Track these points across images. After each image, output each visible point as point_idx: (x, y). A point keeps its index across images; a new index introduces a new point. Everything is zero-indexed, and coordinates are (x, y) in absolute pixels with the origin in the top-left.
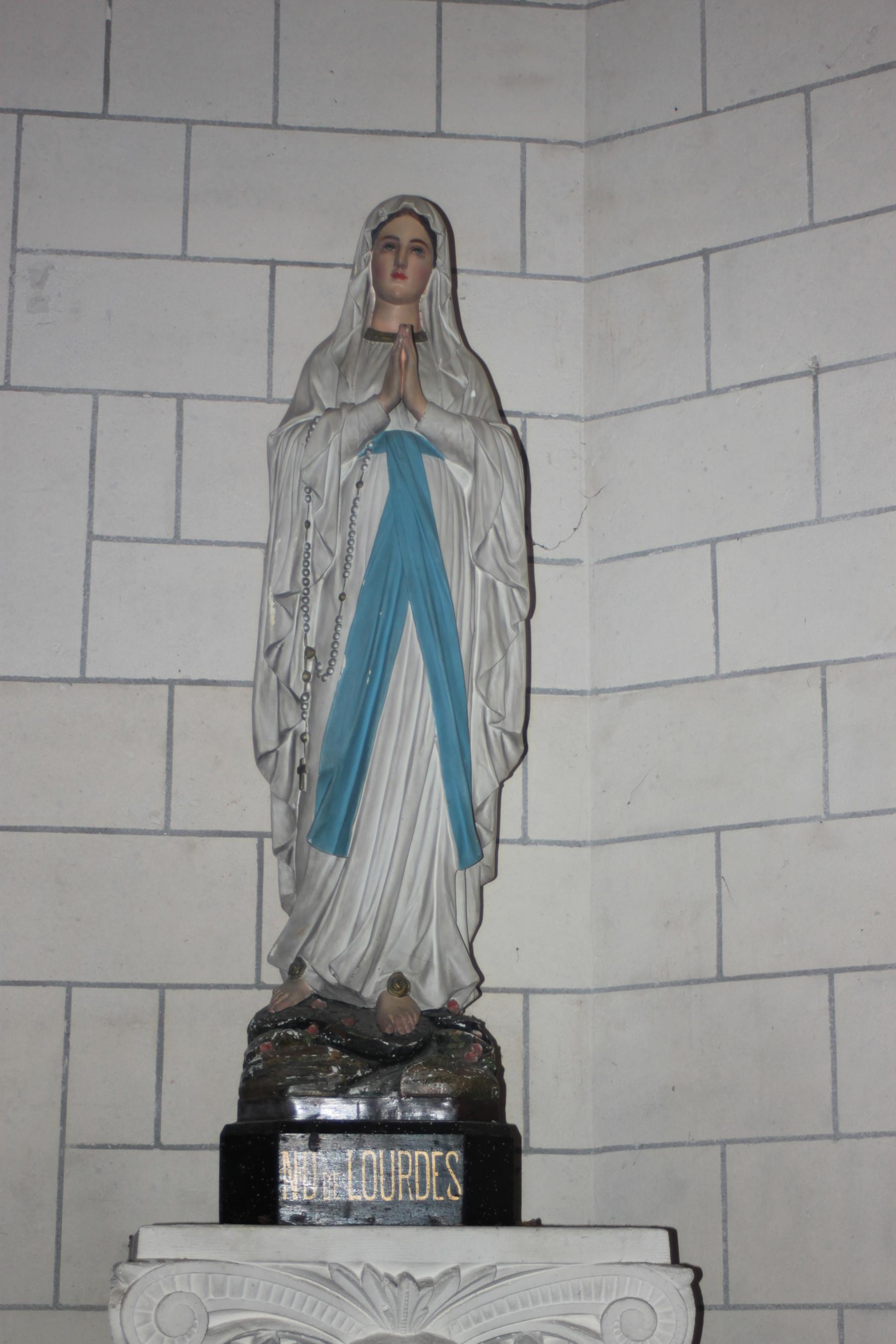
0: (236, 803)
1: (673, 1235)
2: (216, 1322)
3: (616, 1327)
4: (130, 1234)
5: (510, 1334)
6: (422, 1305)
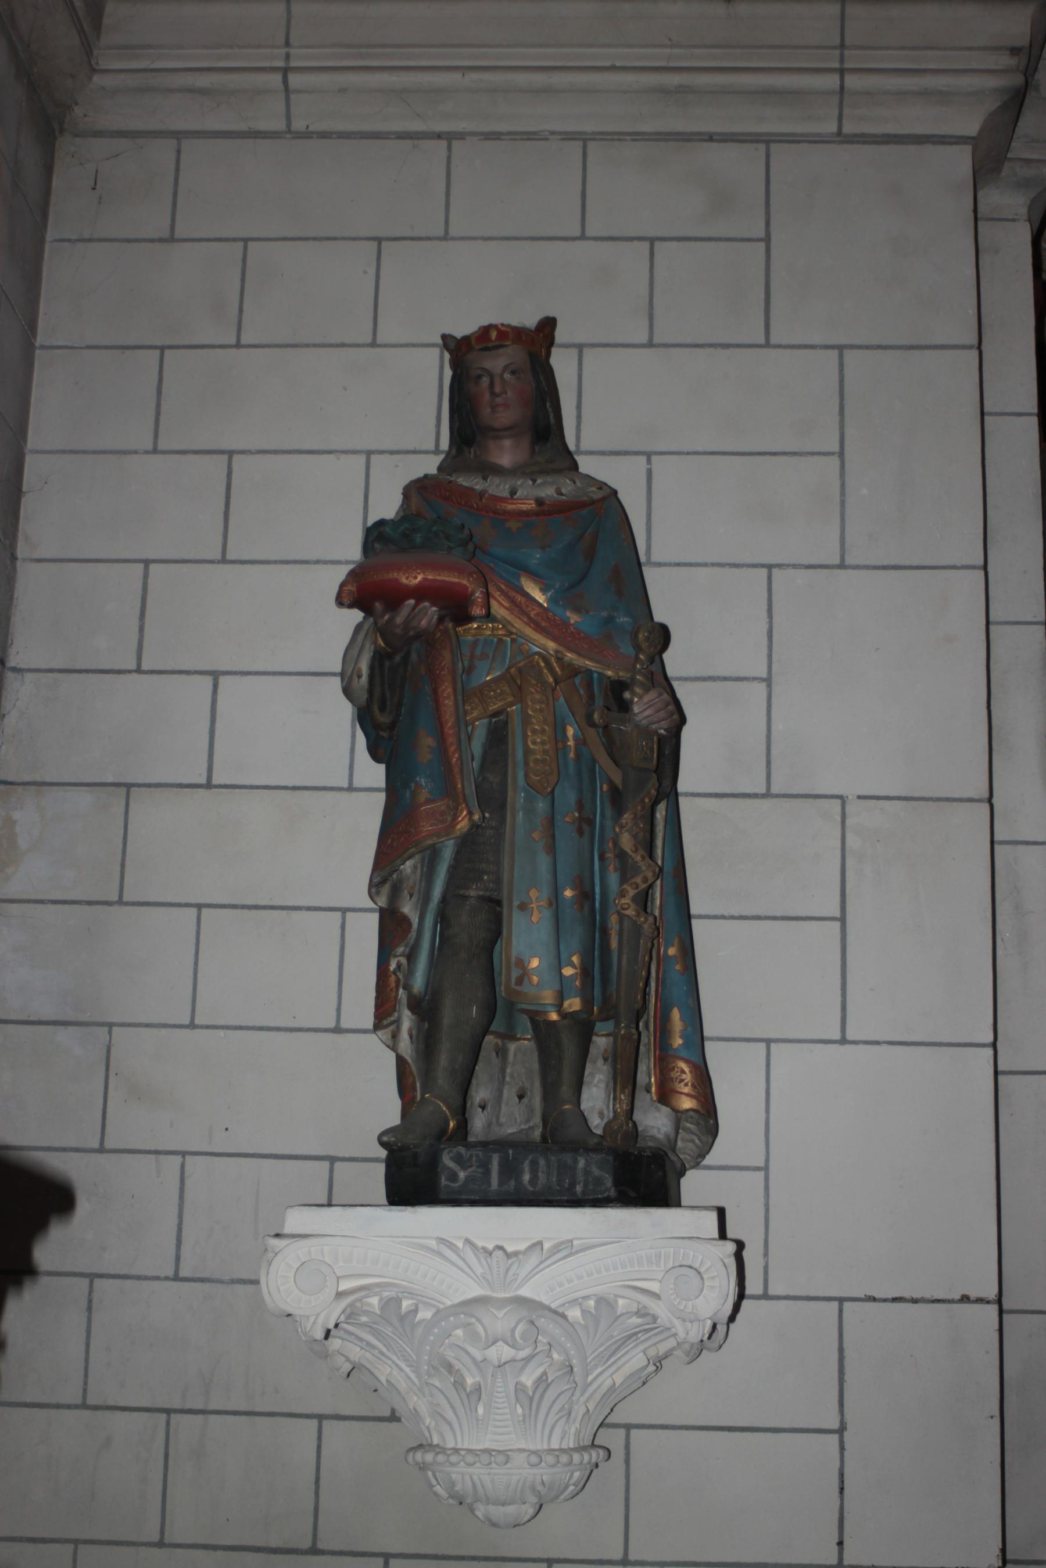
0: (490, 1520)
1: (721, 1213)
2: (344, 1286)
3: (671, 1289)
4: (83, 1206)
5: (589, 1296)
6: (511, 1273)
